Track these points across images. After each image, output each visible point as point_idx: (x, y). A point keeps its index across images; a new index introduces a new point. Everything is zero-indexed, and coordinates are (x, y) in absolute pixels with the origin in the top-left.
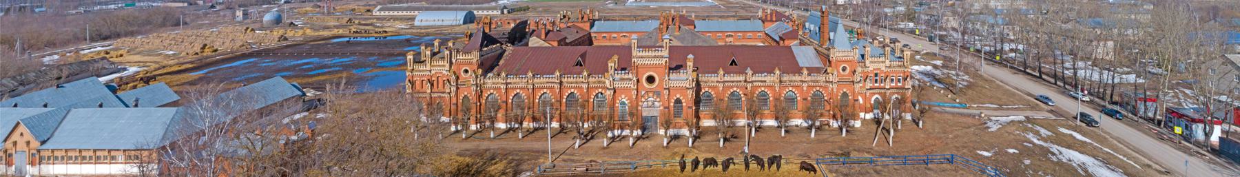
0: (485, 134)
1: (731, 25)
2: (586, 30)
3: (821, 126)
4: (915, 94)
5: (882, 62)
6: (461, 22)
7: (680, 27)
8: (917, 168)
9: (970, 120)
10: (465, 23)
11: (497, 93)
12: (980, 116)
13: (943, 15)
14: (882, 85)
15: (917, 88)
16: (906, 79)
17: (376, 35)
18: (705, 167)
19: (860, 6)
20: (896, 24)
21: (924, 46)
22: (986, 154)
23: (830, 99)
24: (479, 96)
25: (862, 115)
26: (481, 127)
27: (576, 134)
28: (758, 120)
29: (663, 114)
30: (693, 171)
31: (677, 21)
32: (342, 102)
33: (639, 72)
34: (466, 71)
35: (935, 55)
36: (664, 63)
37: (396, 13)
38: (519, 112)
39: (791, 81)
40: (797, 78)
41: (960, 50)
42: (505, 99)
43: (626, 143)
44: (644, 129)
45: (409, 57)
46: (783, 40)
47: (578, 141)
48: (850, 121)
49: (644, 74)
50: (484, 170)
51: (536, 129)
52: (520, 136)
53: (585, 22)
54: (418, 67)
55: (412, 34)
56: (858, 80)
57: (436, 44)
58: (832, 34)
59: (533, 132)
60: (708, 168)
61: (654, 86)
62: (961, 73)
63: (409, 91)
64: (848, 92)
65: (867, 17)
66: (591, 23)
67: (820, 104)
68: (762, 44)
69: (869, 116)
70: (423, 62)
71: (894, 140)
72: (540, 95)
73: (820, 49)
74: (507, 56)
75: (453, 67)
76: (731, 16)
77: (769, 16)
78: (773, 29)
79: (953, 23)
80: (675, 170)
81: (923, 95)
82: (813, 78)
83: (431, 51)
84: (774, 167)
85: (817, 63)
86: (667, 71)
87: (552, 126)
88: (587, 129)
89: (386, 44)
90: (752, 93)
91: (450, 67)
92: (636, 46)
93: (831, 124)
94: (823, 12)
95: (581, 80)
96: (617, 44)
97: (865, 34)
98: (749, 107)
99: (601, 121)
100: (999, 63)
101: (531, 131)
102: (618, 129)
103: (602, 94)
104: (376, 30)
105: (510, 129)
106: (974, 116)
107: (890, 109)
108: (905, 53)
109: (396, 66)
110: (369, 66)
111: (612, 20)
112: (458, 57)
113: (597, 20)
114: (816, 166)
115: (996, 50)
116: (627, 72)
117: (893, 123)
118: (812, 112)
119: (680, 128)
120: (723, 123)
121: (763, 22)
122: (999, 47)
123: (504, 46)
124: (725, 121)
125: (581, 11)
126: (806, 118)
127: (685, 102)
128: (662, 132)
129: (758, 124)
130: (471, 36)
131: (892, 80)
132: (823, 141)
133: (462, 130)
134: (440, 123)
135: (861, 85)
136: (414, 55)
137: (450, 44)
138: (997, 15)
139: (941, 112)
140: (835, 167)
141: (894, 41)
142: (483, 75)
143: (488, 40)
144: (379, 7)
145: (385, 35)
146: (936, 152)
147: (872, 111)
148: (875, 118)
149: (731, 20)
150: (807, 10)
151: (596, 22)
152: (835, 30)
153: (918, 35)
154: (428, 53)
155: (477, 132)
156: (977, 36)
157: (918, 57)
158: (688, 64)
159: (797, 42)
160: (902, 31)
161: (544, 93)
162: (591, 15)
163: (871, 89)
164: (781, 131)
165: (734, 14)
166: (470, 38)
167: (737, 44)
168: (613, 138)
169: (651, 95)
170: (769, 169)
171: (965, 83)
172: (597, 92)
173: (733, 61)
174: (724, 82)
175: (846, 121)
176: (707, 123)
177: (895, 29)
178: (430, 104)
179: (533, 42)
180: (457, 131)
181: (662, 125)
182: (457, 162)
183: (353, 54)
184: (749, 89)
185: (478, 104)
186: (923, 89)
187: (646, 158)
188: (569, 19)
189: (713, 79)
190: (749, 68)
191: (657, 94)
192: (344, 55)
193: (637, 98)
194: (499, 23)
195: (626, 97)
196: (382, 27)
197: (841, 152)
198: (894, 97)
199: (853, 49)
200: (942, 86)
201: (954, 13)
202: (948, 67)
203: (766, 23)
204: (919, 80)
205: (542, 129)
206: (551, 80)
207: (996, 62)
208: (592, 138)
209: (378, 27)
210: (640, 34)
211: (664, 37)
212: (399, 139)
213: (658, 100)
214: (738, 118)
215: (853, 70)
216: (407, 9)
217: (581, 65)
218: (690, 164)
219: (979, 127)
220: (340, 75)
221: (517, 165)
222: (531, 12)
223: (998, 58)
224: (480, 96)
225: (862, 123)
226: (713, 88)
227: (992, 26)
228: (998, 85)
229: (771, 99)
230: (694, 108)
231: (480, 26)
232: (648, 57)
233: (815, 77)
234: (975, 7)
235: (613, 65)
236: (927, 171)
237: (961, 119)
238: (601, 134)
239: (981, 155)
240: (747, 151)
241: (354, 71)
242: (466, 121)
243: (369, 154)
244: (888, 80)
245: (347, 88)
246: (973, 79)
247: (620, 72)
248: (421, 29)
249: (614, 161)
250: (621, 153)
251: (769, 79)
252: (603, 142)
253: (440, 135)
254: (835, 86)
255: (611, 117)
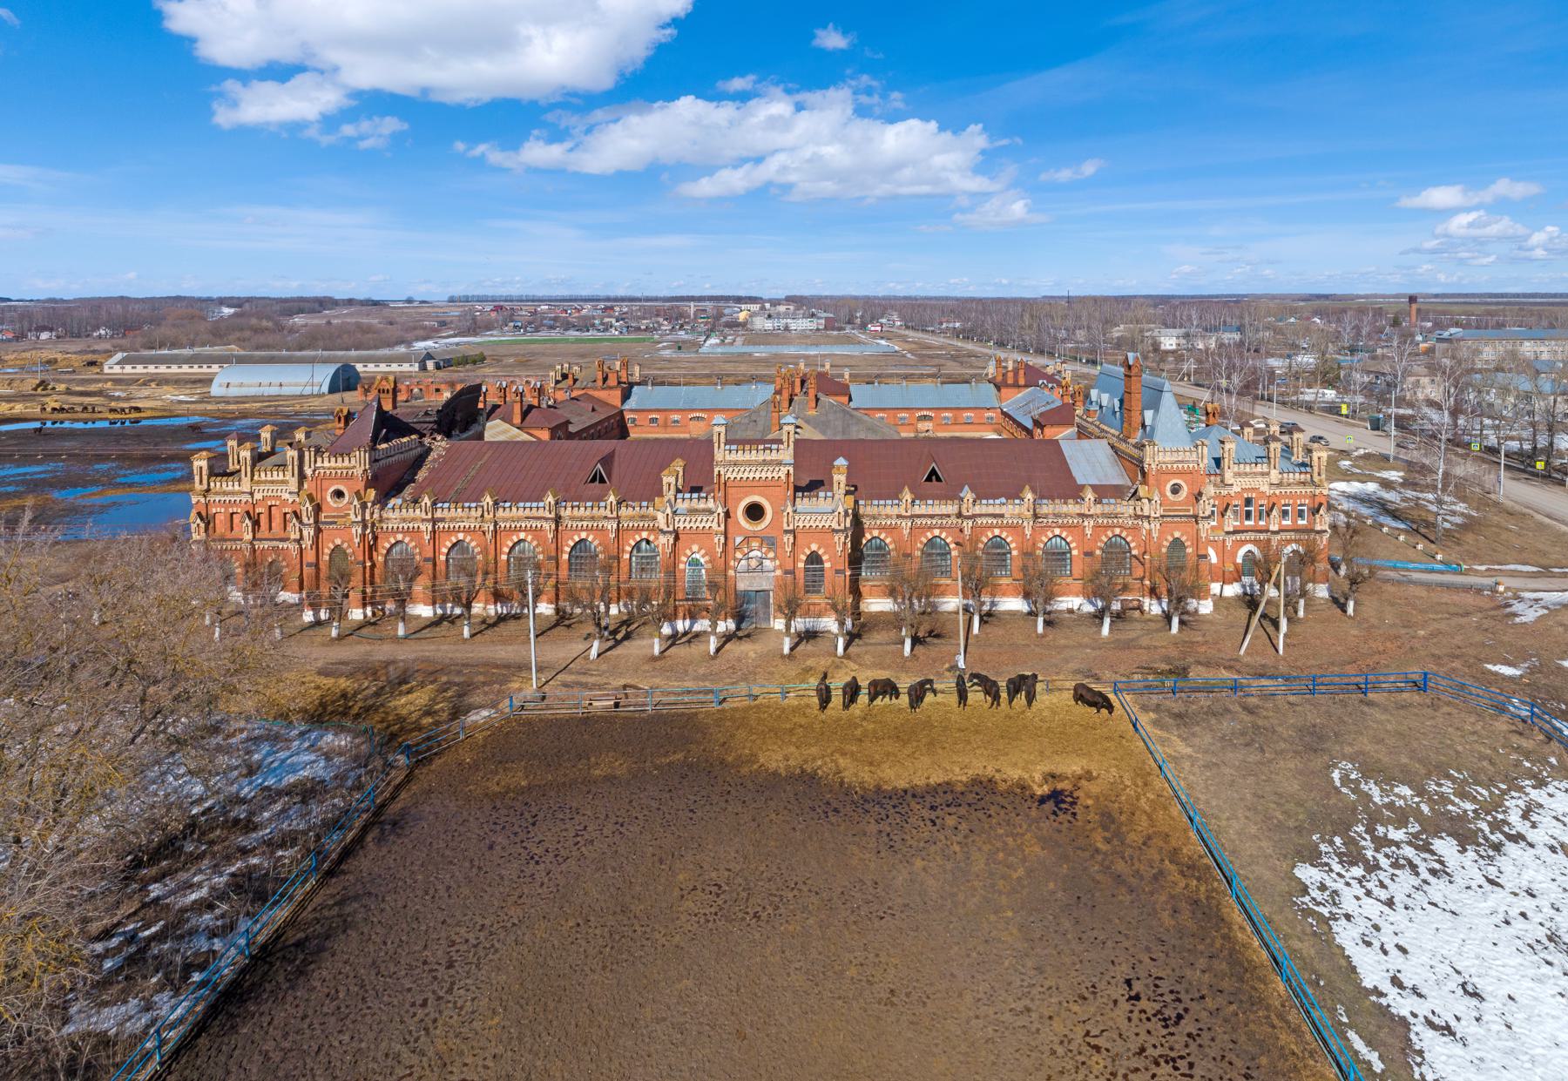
0: (386, 629)
1: (927, 394)
2: (615, 407)
3: (1124, 610)
4: (1338, 543)
5: (1263, 474)
6: (325, 389)
7: (817, 400)
8: (1340, 700)
9: (1469, 600)
10: (333, 389)
11: (411, 540)
12: (1494, 590)
13: (1407, 373)
14: (1262, 523)
15: (1342, 530)
16: (1318, 511)
17: (111, 416)
18: (872, 699)
19: (1213, 354)
20: (1296, 393)
21: (1361, 439)
22: (217, 635)
23: (1145, 553)
24: (370, 547)
25: (1215, 588)
26: (374, 614)
27: (592, 629)
28: (986, 599)
29: (781, 585)
30: (846, 707)
31: (811, 385)
32: (24, 560)
33: (729, 497)
34: (339, 494)
35: (1386, 458)
36: (783, 477)
37: (163, 369)
38: (463, 582)
39: (1057, 515)
40: (1071, 508)
41: (1446, 449)
42: (430, 555)
43: (702, 647)
44: (740, 618)
45: (196, 464)
46: (1042, 427)
47: (596, 644)
48: (1189, 600)
49: (741, 500)
50: (382, 705)
51: (501, 619)
52: (466, 632)
53: (611, 388)
54: (216, 485)
55: (204, 413)
56: (1208, 513)
57: (266, 434)
58: (1149, 414)
59: (494, 625)
60: (878, 701)
61: (763, 526)
62: (1446, 499)
63: (198, 535)
64: (1183, 539)
65: (1228, 377)
66: (623, 389)
67: (1121, 565)
68: (995, 436)
69: (1232, 590)
70: (232, 474)
71: (1288, 641)
72: (511, 544)
73: (1123, 446)
74: (434, 460)
75: (306, 486)
76: (929, 376)
77: (1010, 375)
78: (1019, 402)
79: (1430, 389)
80: (808, 706)
81: (1356, 545)
82: (1107, 509)
83: (252, 450)
84: (1021, 699)
85: (1114, 475)
86: (790, 493)
87: (537, 611)
88: (615, 617)
89: (141, 436)
90: (974, 540)
91: (301, 484)
92: (723, 439)
93: (1146, 608)
94: (1129, 367)
95: (602, 512)
96: (682, 436)
97: (1223, 414)
98: (966, 570)
99: (648, 600)
100: (1544, 477)
101: (491, 621)
102: (684, 619)
103: (648, 542)
104: (113, 404)
105: (443, 618)
106: (1479, 591)
107: (1279, 574)
108: (1315, 455)
109: (162, 482)
110: (94, 482)
111: (671, 384)
112: (319, 464)
113: (639, 384)
114: (1111, 696)
115: (1535, 448)
116: (703, 495)
117: (1285, 605)
118: (1105, 580)
119: (819, 616)
120: (912, 604)
121: (999, 389)
122: (1542, 442)
123: (427, 441)
124: (915, 601)
125: (601, 364)
126: (1090, 596)
127: (829, 560)
128: (779, 624)
129: (986, 608)
130: (349, 417)
131: (1285, 513)
132: (1128, 645)
133: (329, 621)
134: (276, 605)
135: (1214, 523)
136: (209, 459)
137: (300, 435)
138: (1538, 372)
139: (1399, 582)
140: (1155, 699)
141: (1289, 429)
142: (379, 502)
143: (389, 426)
144: (119, 356)
145: (135, 415)
146: (1387, 666)
147: (1238, 580)
148: (1245, 594)
149: (928, 384)
150: (1094, 363)
151: (635, 388)
152: (1155, 405)
153: (1347, 416)
154: (246, 454)
155: (366, 624)
156: (1489, 417)
157: (1345, 464)
158: (836, 477)
159: (1073, 430)
160: (1309, 407)
161: (520, 541)
162: (623, 374)
163: (1235, 532)
164: (1036, 621)
165: (934, 370)
166: (347, 423)
167: (940, 435)
168: (674, 638)
169: (755, 544)
170: (1011, 702)
171: (1458, 520)
172: (638, 539)
173: (933, 472)
174: (912, 516)
175: (1178, 601)
176: (877, 604)
177: (1293, 403)
178: (250, 566)
179: (494, 431)
180: (318, 623)
181: (780, 609)
182: (318, 687)
183: (50, 457)
184: (967, 532)
185: (368, 564)
186: (1355, 532)
187: (745, 679)
188: (575, 381)
189: (888, 510)
190: (966, 487)
191: (769, 542)
192: (28, 459)
193: (725, 551)
194: (416, 390)
195: (700, 549)
196: (128, 399)
197: (1168, 667)
198: (1289, 549)
199: (1196, 446)
200: (1402, 526)
201: (1433, 369)
202: (1416, 484)
203: (1003, 390)
204: (1347, 514)
205: (517, 617)
206: (534, 513)
207: (1537, 475)
208: (627, 637)
209: (118, 399)
210: (733, 413)
211: (782, 421)
212: (174, 639)
213: (771, 555)
214: (943, 594)
215: (1196, 492)
216: (190, 360)
217: (602, 481)
218: (840, 692)
219: (1493, 613)
220: (16, 502)
221: (460, 695)
222: (490, 366)
223: (1540, 465)
224: (372, 548)
225: (1215, 605)
226: (890, 529)
227: (1528, 397)
228: (1541, 525)
229: (1015, 553)
230: (848, 573)
231: (371, 396)
232: (749, 463)
233: (1110, 506)
234: (1484, 356)
235: (672, 480)
236: (1366, 709)
237: (1446, 597)
238: (647, 630)
239: (1496, 674)
240: (961, 664)
241: (56, 495)
242: (339, 600)
243: (97, 672)
244: (1274, 512)
245: (36, 529)
246: (1478, 510)
247: (687, 495)
248: (228, 403)
249: (675, 685)
250: (690, 669)
251: (1010, 510)
252: (652, 646)
253: (278, 631)
254: (1155, 527)
255: (670, 592)
